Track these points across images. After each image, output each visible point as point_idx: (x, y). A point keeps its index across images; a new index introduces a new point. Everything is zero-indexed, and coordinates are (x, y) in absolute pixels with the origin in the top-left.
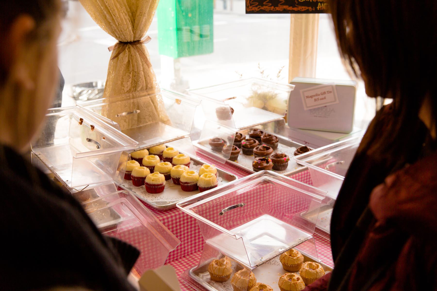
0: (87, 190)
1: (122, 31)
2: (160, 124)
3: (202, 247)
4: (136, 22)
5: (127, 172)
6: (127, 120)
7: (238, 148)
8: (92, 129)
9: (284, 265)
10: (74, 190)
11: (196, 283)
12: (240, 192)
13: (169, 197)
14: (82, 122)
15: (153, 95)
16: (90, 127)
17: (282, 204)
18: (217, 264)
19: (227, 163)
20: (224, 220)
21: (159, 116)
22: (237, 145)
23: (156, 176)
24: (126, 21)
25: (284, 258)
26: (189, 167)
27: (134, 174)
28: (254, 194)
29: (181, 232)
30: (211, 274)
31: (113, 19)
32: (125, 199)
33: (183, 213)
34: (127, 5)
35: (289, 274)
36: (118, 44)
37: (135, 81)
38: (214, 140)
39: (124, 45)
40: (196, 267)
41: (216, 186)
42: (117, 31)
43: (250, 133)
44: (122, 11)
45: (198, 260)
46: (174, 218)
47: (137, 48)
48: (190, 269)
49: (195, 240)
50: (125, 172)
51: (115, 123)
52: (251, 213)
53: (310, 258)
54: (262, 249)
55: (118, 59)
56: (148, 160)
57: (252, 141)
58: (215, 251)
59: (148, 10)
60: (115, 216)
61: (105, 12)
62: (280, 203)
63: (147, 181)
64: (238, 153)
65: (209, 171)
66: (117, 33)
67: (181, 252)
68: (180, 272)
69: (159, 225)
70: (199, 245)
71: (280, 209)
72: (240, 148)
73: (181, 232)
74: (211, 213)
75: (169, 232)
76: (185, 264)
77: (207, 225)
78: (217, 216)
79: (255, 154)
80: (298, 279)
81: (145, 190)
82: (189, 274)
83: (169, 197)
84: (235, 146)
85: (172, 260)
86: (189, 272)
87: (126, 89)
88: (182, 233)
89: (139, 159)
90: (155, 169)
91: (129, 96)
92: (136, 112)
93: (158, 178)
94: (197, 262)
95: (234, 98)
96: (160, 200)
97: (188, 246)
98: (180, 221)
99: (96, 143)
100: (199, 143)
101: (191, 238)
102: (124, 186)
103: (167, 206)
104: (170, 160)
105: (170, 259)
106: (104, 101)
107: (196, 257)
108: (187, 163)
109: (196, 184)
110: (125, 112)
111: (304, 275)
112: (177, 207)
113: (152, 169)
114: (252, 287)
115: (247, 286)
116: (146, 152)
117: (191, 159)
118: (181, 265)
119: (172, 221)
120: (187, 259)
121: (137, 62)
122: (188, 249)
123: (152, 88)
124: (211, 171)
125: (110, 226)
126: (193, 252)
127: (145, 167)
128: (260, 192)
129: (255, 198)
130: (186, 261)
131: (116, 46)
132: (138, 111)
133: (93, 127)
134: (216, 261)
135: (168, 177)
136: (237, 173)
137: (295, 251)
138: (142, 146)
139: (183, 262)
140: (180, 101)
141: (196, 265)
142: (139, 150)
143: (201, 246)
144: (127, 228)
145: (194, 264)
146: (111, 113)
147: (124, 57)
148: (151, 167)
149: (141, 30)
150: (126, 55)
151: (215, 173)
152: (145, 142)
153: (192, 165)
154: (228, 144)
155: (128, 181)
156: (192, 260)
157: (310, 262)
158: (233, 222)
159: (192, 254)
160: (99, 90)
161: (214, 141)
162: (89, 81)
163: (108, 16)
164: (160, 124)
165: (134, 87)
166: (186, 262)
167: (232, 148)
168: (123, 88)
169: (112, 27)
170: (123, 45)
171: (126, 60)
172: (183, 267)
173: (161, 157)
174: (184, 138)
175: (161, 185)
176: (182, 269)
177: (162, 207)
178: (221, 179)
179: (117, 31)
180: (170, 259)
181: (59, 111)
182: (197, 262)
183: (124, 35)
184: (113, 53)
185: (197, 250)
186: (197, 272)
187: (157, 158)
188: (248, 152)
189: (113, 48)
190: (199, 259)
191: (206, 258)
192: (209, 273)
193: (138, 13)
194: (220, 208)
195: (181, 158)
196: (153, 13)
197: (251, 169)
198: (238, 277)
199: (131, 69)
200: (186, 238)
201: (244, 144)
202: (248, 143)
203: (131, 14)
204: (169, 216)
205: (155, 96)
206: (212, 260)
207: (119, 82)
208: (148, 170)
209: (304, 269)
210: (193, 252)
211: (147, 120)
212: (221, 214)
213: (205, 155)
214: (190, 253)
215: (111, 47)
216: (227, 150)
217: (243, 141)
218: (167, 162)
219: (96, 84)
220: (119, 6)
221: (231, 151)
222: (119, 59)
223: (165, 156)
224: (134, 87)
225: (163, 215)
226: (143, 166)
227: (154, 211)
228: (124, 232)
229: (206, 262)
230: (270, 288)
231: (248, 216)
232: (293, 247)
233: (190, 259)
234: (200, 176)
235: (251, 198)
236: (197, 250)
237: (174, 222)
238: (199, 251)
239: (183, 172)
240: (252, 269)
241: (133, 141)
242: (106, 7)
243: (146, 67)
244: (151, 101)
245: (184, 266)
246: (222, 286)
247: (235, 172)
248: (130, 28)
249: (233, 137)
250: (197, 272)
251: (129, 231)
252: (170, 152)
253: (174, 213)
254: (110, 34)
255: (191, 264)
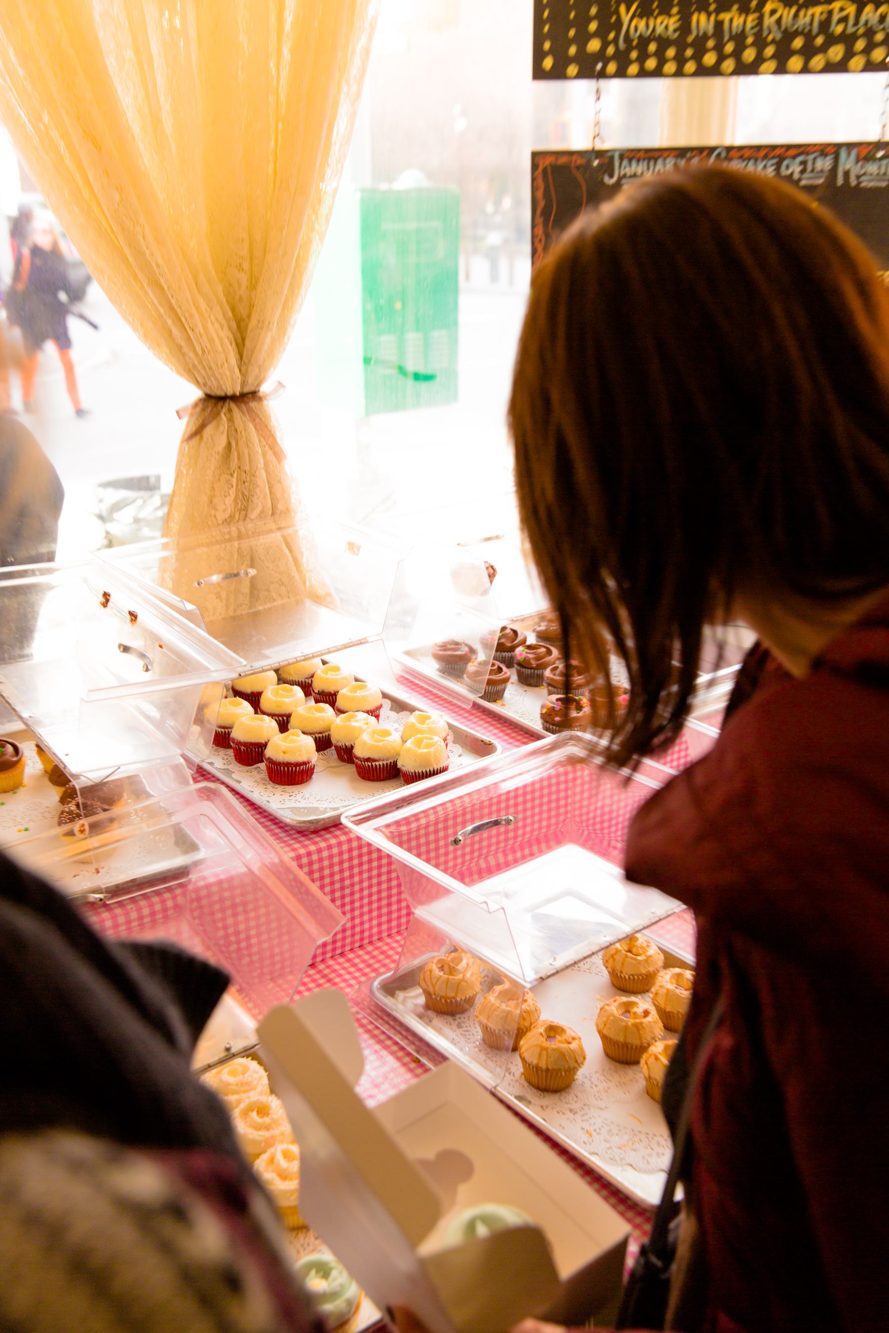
0: (112, 781)
1: (210, 368)
2: (308, 603)
3: (408, 922)
4: (247, 343)
5: (220, 727)
6: (224, 595)
7: (504, 668)
8: (132, 620)
9: (613, 974)
10: (83, 778)
11: (389, 1015)
12: (506, 787)
13: (327, 795)
14: (107, 601)
15: (290, 531)
16: (129, 617)
17: (614, 815)
18: (442, 968)
19: (476, 706)
20: (489, 846)
21: (305, 583)
22: (503, 661)
23: (293, 741)
24: (222, 344)
25: (612, 956)
26: (377, 717)
27: (238, 734)
28: (542, 788)
29: (352, 885)
30: (427, 993)
31: (189, 338)
32: (209, 803)
33: (359, 838)
34: (224, 301)
35: (625, 999)
36: (201, 400)
37: (243, 494)
38: (444, 647)
39: (216, 405)
40: (389, 974)
41: (444, 769)
42: (200, 367)
43: (539, 629)
44: (213, 318)
45: (396, 957)
46: (335, 851)
47: (250, 411)
48: (375, 978)
49: (389, 905)
50: (215, 728)
51: (189, 606)
52: (473, 864)
53: (679, 959)
54: (558, 933)
55: (201, 438)
56: (274, 698)
57: (543, 650)
58: (436, 938)
59: (277, 314)
60: (185, 843)
61: (169, 322)
62: (611, 812)
63: (269, 752)
64: (506, 680)
65: (422, 731)
66: (199, 372)
67: (353, 935)
68: (350, 986)
69: (288, 870)
70: (399, 918)
71: (602, 829)
72: (509, 666)
73: (352, 885)
74: (432, 837)
75: (314, 888)
76: (362, 966)
77: (413, 871)
78: (446, 846)
79: (549, 685)
80: (646, 1013)
81: (265, 774)
82: (371, 992)
83: (327, 795)
84: (497, 663)
85: (329, 955)
86: (371, 985)
87: (221, 516)
88: (357, 888)
89: (253, 694)
90: (293, 720)
91: (229, 533)
92: (247, 574)
93: (296, 746)
94: (394, 961)
95: (497, 537)
96: (303, 804)
97: (370, 920)
98: (351, 859)
99: (142, 656)
100: (408, 653)
101: (379, 900)
102: (211, 764)
103: (318, 821)
104: (329, 698)
105: (324, 953)
106: (165, 547)
107: (392, 948)
108: (372, 707)
109: (395, 764)
110: (219, 573)
111: (661, 1002)
112: (341, 824)
113: (284, 723)
114: (528, 1029)
115: (515, 1026)
116: (273, 676)
117: (385, 696)
118: (352, 970)
119: (331, 857)
120: (368, 953)
121: (248, 446)
122: (371, 928)
123: (287, 511)
124: (432, 731)
125: (169, 871)
126: (385, 934)
127: (266, 717)
128: (558, 784)
129: (545, 799)
130: (366, 957)
131: (196, 405)
132: (252, 572)
133: (133, 616)
134: (439, 961)
135: (323, 743)
136: (501, 734)
137: (641, 940)
138: (258, 665)
139: (357, 961)
140: (359, 548)
141: (389, 970)
142: (252, 674)
143: (404, 920)
144: (216, 875)
145: (384, 966)
146: (182, 578)
147: (217, 435)
148: (282, 716)
149: (260, 367)
150: (222, 428)
151: (444, 734)
152: (267, 652)
153: (385, 712)
154: (481, 656)
155: (222, 751)
156: (381, 957)
157: (677, 970)
158: (505, 855)
159: (380, 939)
160: (163, 496)
161: (445, 650)
162: (136, 472)
163: (175, 332)
164: (308, 603)
165: (240, 510)
166: (364, 961)
167: (489, 668)
168: (213, 512)
169: (187, 357)
170: (215, 402)
171: (223, 441)
172: (357, 974)
173: (307, 688)
174: (366, 642)
175: (305, 763)
176: (355, 978)
177: (304, 822)
178: (458, 749)
179: (200, 367)
180: (324, 953)
181: (49, 571)
182: (394, 961)
183: (216, 379)
184: (187, 425)
185: (394, 931)
186: (390, 988)
187: (298, 691)
188: (530, 677)
189: (189, 410)
190: (397, 953)
191: (416, 952)
192: (420, 991)
193: (253, 323)
194: (455, 825)
195: (359, 693)
196: (292, 321)
197: (537, 725)
198: (493, 1005)
199: (234, 463)
200: (545, 815)
201: (521, 659)
202: (531, 656)
203: (234, 325)
204: (323, 845)
205: (296, 532)
206: (428, 958)
207: (205, 499)
208: (274, 724)
209: (661, 987)
210: (385, 934)
211: (274, 595)
212: (456, 842)
213: (421, 684)
214: (375, 938)
215: (185, 409)
216: (477, 673)
217: (520, 650)
218: (321, 704)
219: (158, 478)
220: (203, 305)
221: (487, 677)
222: (205, 439)
223: (317, 686)
224: (240, 510)
225: (307, 842)
226: (264, 713)
227: (286, 831)
228: (208, 886)
229: (416, 962)
230: (573, 1034)
231: (466, 873)
232: (637, 932)
233: (376, 953)
234: (404, 742)
235: (533, 800)
236: (394, 931)
237: (336, 860)
238: (399, 933)
239: (361, 731)
240: (528, 986)
241: (232, 658)
242: (171, 308)
243: (274, 459)
244: (284, 546)
245: (360, 970)
246: (455, 1024)
247: (496, 731)
248: (233, 361)
249: (492, 639)
250: (390, 988)
251: (220, 883)
252: (331, 676)
253: (336, 837)
254: (181, 375)
255: (377, 965)
